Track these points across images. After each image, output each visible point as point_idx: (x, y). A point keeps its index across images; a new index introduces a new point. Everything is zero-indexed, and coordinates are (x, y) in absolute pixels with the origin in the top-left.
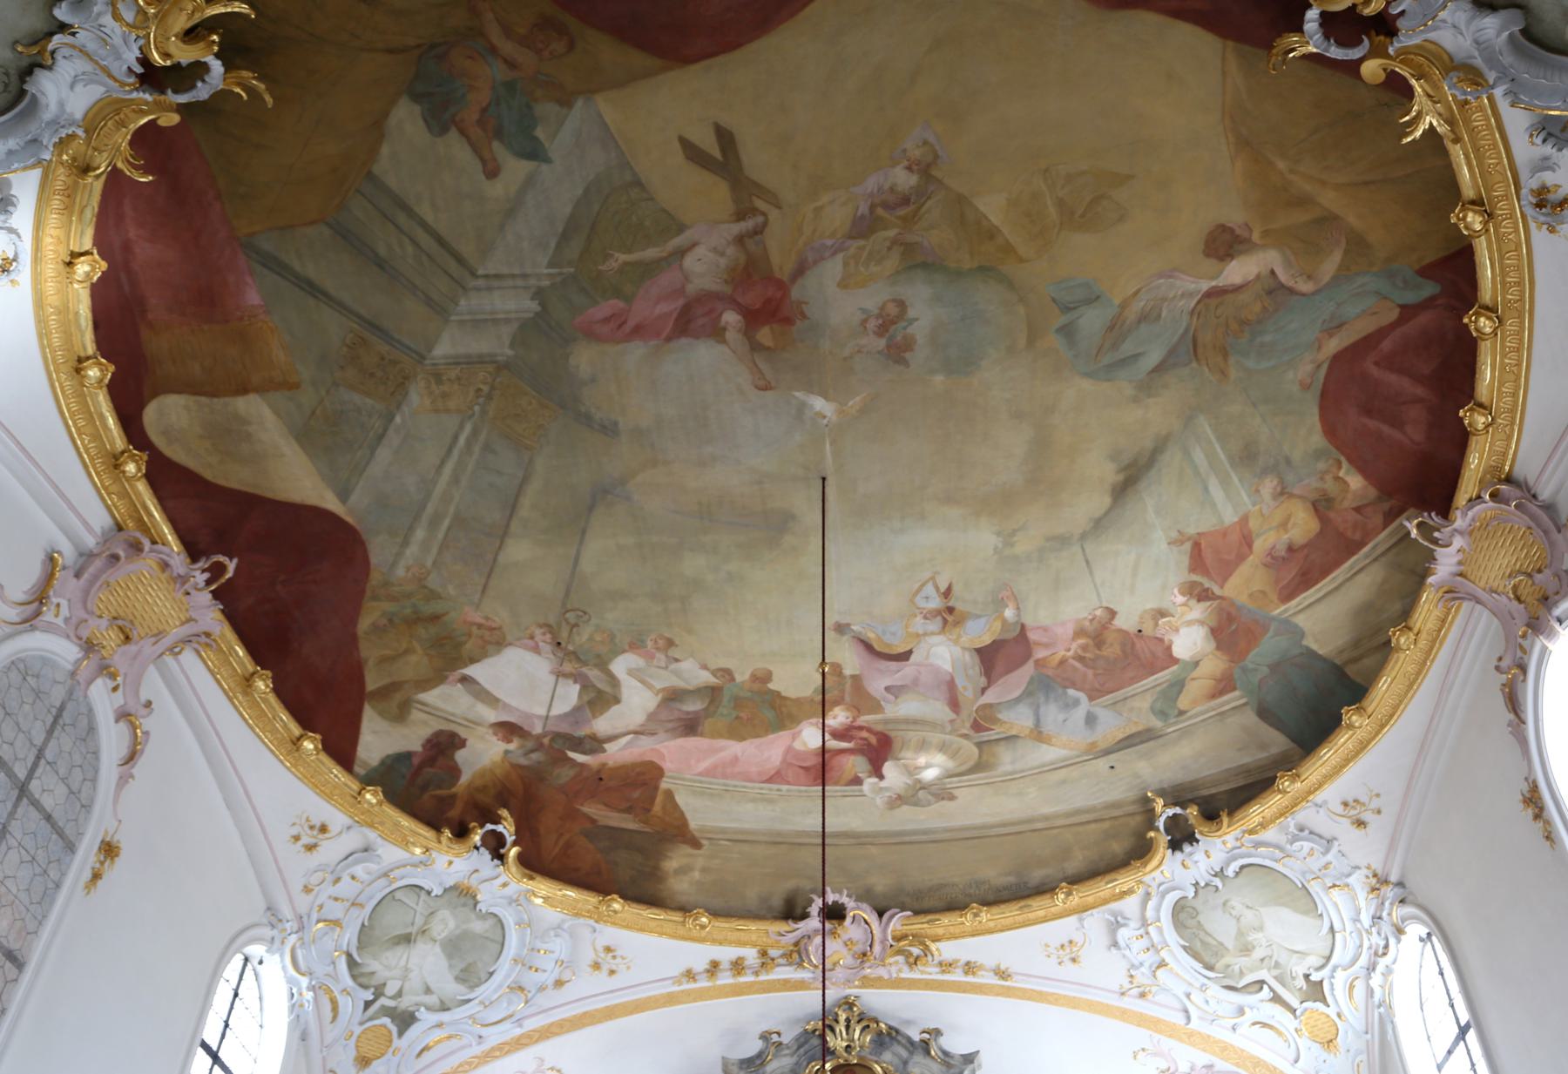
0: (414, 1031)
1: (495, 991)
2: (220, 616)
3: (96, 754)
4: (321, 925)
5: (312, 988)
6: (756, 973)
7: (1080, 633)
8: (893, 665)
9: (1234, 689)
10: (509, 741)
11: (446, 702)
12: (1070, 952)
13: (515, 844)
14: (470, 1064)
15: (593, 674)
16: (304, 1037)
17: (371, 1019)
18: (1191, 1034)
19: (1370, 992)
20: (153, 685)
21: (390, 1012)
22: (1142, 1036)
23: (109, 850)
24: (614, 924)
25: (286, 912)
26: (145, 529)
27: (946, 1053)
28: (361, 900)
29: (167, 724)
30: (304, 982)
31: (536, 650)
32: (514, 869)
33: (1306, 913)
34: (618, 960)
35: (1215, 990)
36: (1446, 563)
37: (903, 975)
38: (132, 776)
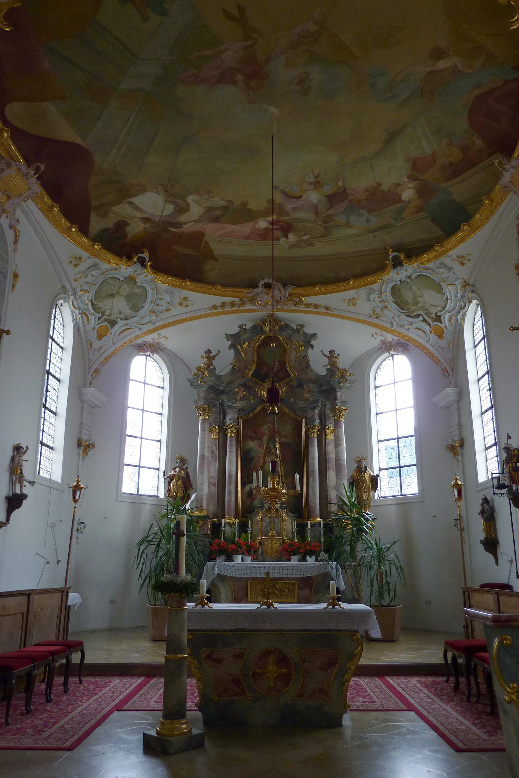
0: (116, 327)
1: (145, 313)
2: (40, 186)
3: (6, 242)
4: (82, 292)
5: (80, 314)
6: (239, 307)
7: (366, 190)
8: (295, 200)
9: (424, 211)
10: (146, 224)
11: (122, 210)
12: (353, 302)
13: (149, 261)
14: (137, 337)
15: (180, 202)
16: (78, 330)
17: (101, 323)
18: (393, 331)
19: (457, 320)
20: (19, 214)
21: (106, 320)
22: (377, 331)
23: (16, 276)
24: (187, 290)
25: (69, 288)
26: (11, 157)
27: (305, 333)
28: (95, 283)
29: (24, 226)
30: (77, 312)
31: (158, 193)
32: (150, 271)
33: (438, 292)
34: (189, 302)
35: (403, 317)
36: (506, 177)
37: (291, 308)
38: (17, 248)
